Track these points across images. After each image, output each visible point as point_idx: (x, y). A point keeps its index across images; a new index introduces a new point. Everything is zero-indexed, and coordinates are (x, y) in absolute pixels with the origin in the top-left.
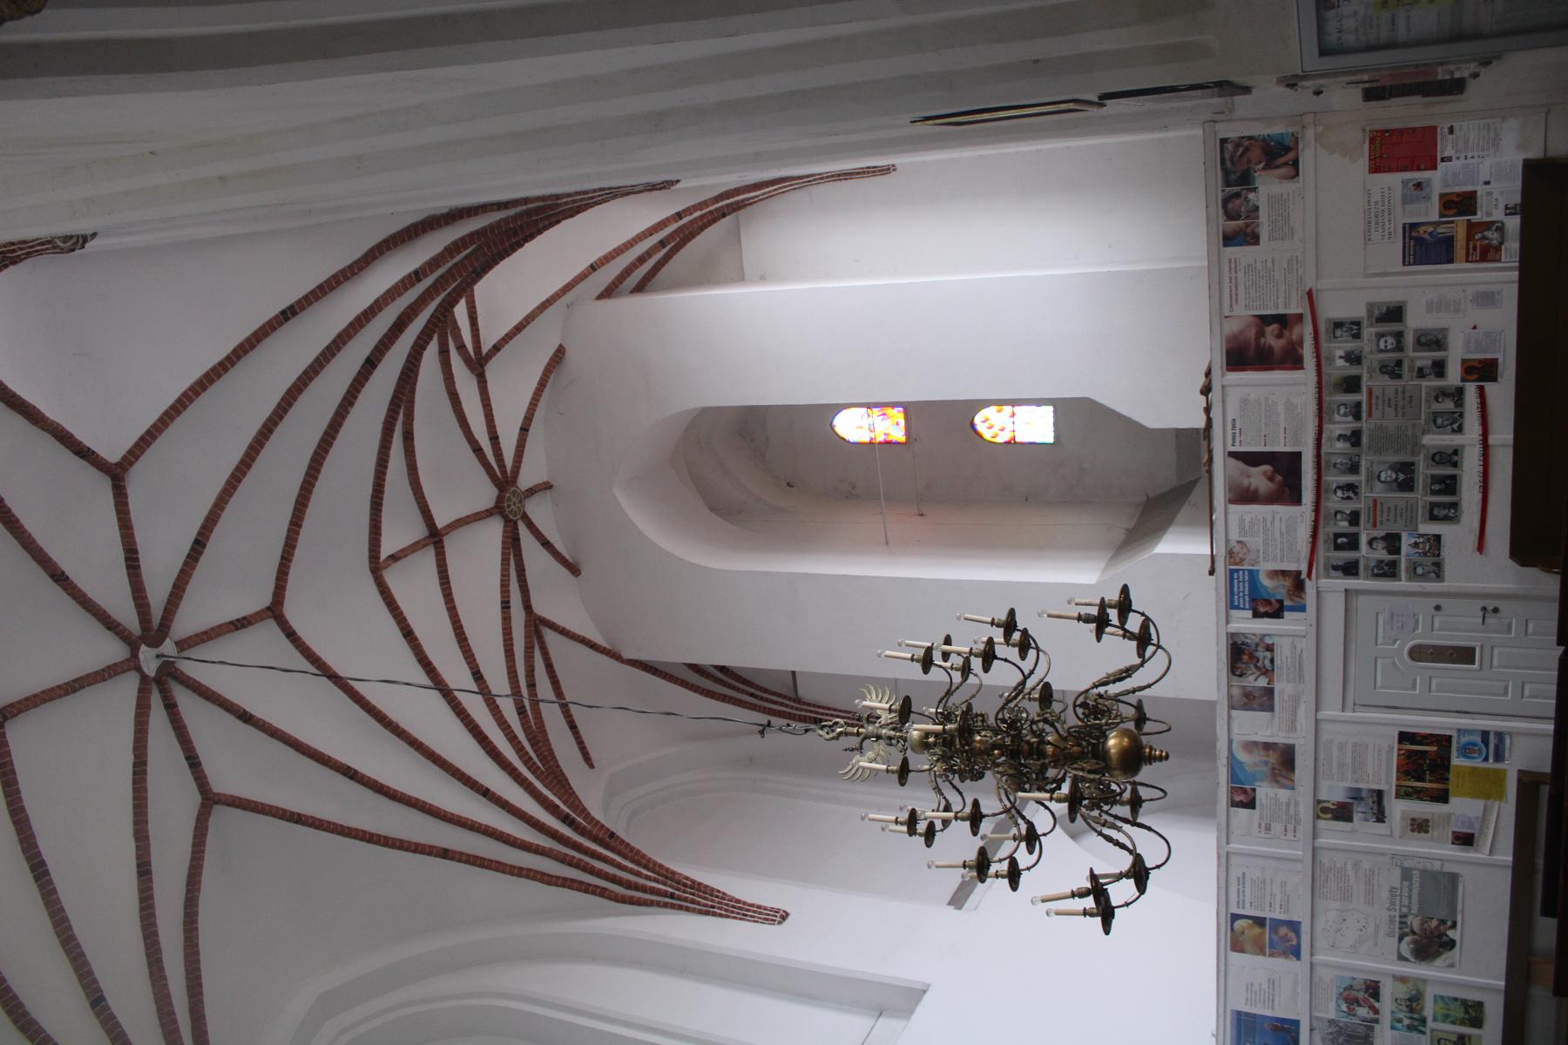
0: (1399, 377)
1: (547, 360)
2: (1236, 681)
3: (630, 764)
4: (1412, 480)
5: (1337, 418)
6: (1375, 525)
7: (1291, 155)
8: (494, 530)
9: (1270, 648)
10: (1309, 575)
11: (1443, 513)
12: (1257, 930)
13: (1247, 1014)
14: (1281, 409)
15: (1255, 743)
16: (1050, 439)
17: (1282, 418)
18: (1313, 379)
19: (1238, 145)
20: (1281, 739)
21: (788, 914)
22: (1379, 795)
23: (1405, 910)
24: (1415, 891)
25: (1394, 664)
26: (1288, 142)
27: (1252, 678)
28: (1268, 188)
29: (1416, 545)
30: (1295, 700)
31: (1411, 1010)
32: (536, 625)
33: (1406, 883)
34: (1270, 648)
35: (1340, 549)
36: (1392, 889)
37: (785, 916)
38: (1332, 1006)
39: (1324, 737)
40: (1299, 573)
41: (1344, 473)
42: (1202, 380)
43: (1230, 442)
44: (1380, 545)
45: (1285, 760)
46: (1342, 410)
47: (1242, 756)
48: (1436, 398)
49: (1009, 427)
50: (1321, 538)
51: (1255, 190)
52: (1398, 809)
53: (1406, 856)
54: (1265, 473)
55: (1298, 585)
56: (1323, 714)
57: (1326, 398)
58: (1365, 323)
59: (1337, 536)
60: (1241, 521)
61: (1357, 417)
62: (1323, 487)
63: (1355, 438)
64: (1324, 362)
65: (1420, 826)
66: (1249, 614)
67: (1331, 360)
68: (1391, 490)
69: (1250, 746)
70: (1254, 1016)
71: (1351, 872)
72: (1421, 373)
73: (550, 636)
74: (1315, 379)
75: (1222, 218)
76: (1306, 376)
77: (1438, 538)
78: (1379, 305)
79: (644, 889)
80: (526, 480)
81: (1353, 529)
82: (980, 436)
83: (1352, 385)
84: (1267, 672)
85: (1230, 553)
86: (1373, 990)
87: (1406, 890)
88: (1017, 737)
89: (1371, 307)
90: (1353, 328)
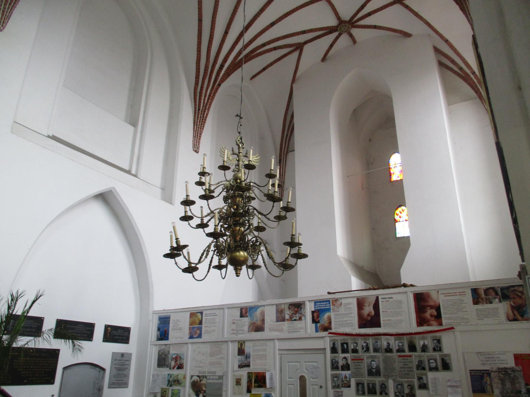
0: (418, 369)
1: (405, 31)
2: (287, 307)
3: (251, 91)
4: (373, 375)
5: (397, 342)
6: (353, 360)
7: (519, 317)
8: (332, 22)
9: (300, 319)
10: (330, 333)
11: (360, 388)
12: (198, 322)
13: (169, 321)
14: (399, 318)
15: (264, 316)
16: (398, 235)
17: (395, 318)
18: (413, 331)
19: (522, 293)
20: (266, 326)
21: (198, 152)
22: (248, 366)
23: (208, 377)
24: (215, 381)
25: (298, 369)
26: (526, 316)
27: (288, 312)
28: (502, 308)
29: (346, 377)
30: (281, 330)
31: (175, 381)
32: (299, 47)
33: (217, 377)
34: (300, 319)
35: (342, 345)
36: (215, 372)
37: (197, 152)
38: (174, 352)
39: (268, 343)
40: (331, 329)
41: (373, 346)
42: (409, 284)
43: (383, 297)
44: (344, 362)
45: (259, 328)
46: (400, 344)
47: (259, 311)
48: (409, 385)
49: (401, 220)
50: (345, 337)
51: (500, 301)
52: (244, 373)
53: (227, 377)
54: (371, 312)
55: (326, 328)
56: (276, 341)
57: (405, 337)
58: (441, 353)
59: (347, 344)
60: (350, 304)
61: (398, 351)
62: (367, 337)
63: (389, 350)
64: (421, 335)
65: (238, 382)
66: (313, 310)
67: (424, 339)
68: (368, 366)
69: (263, 314)
70: (169, 324)
71: (220, 356)
72: (420, 379)
73: (296, 54)
74: (413, 332)
75: (485, 287)
76: (414, 328)
77: (349, 386)
78: (450, 359)
79: (200, 99)
80: (355, 32)
81: (350, 350)
82: (397, 209)
83: (412, 348)
84: (291, 319)
85: (336, 300)
86: (180, 367)
87: (215, 377)
88: (242, 215)
89: (448, 355)
90: (438, 348)
